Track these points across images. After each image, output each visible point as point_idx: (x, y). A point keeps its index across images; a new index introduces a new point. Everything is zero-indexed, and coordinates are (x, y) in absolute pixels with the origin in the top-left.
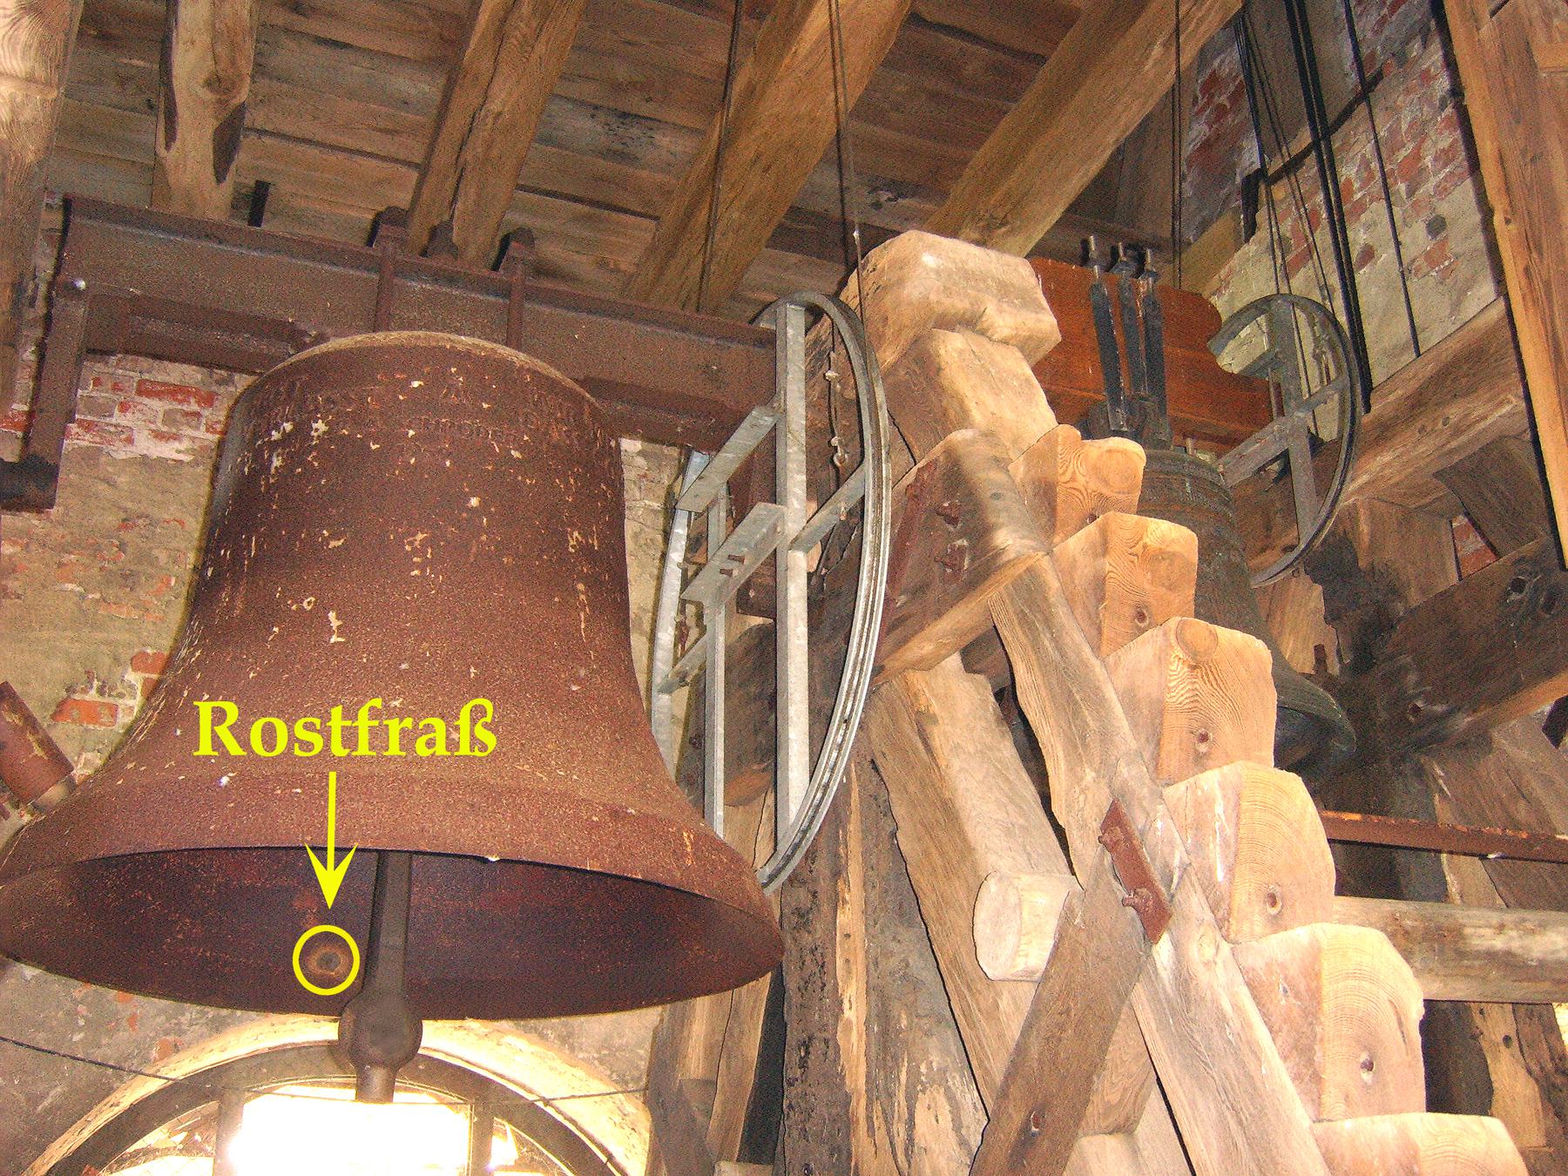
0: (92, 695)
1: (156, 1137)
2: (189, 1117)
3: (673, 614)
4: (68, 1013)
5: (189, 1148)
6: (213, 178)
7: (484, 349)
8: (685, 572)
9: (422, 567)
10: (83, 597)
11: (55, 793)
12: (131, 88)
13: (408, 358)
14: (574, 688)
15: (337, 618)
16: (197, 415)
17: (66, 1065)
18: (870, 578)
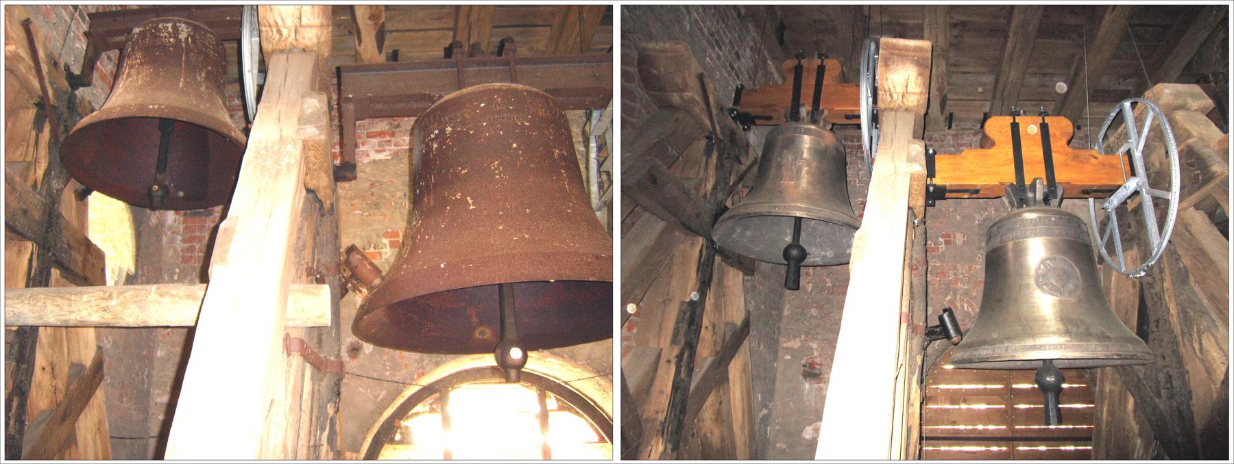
0: (372, 250)
1: (419, 408)
2: (429, 400)
3: (595, 179)
4: (382, 365)
5: (432, 410)
6: (377, 53)
7: (505, 86)
8: (598, 161)
9: (499, 174)
10: (362, 215)
11: (377, 281)
12: (342, 28)
13: (477, 96)
14: (569, 211)
15: (471, 199)
16: (390, 141)
17: (385, 384)
18: (609, 175)
